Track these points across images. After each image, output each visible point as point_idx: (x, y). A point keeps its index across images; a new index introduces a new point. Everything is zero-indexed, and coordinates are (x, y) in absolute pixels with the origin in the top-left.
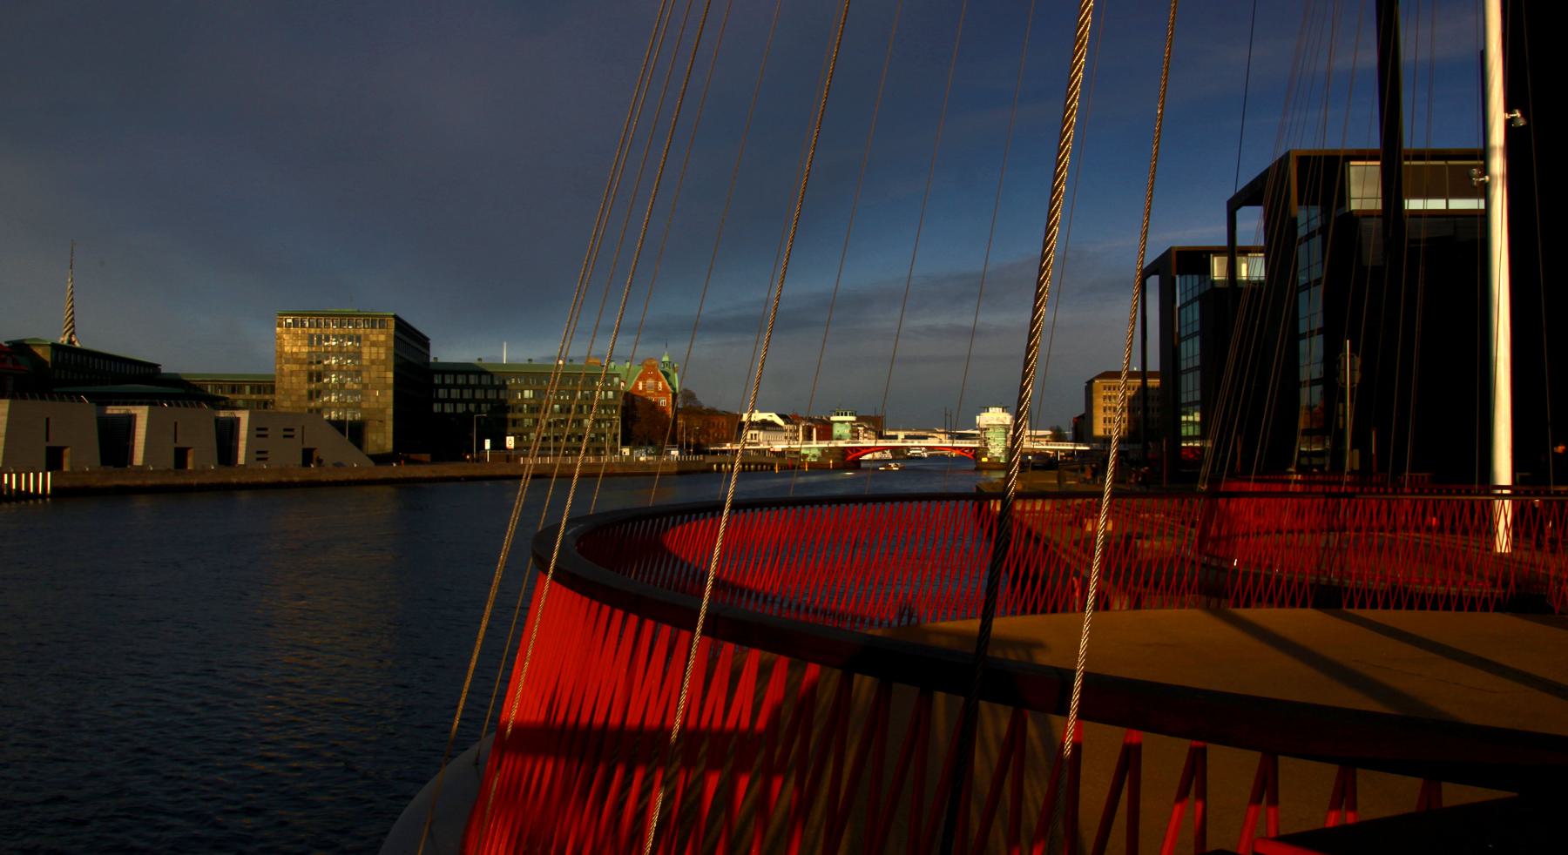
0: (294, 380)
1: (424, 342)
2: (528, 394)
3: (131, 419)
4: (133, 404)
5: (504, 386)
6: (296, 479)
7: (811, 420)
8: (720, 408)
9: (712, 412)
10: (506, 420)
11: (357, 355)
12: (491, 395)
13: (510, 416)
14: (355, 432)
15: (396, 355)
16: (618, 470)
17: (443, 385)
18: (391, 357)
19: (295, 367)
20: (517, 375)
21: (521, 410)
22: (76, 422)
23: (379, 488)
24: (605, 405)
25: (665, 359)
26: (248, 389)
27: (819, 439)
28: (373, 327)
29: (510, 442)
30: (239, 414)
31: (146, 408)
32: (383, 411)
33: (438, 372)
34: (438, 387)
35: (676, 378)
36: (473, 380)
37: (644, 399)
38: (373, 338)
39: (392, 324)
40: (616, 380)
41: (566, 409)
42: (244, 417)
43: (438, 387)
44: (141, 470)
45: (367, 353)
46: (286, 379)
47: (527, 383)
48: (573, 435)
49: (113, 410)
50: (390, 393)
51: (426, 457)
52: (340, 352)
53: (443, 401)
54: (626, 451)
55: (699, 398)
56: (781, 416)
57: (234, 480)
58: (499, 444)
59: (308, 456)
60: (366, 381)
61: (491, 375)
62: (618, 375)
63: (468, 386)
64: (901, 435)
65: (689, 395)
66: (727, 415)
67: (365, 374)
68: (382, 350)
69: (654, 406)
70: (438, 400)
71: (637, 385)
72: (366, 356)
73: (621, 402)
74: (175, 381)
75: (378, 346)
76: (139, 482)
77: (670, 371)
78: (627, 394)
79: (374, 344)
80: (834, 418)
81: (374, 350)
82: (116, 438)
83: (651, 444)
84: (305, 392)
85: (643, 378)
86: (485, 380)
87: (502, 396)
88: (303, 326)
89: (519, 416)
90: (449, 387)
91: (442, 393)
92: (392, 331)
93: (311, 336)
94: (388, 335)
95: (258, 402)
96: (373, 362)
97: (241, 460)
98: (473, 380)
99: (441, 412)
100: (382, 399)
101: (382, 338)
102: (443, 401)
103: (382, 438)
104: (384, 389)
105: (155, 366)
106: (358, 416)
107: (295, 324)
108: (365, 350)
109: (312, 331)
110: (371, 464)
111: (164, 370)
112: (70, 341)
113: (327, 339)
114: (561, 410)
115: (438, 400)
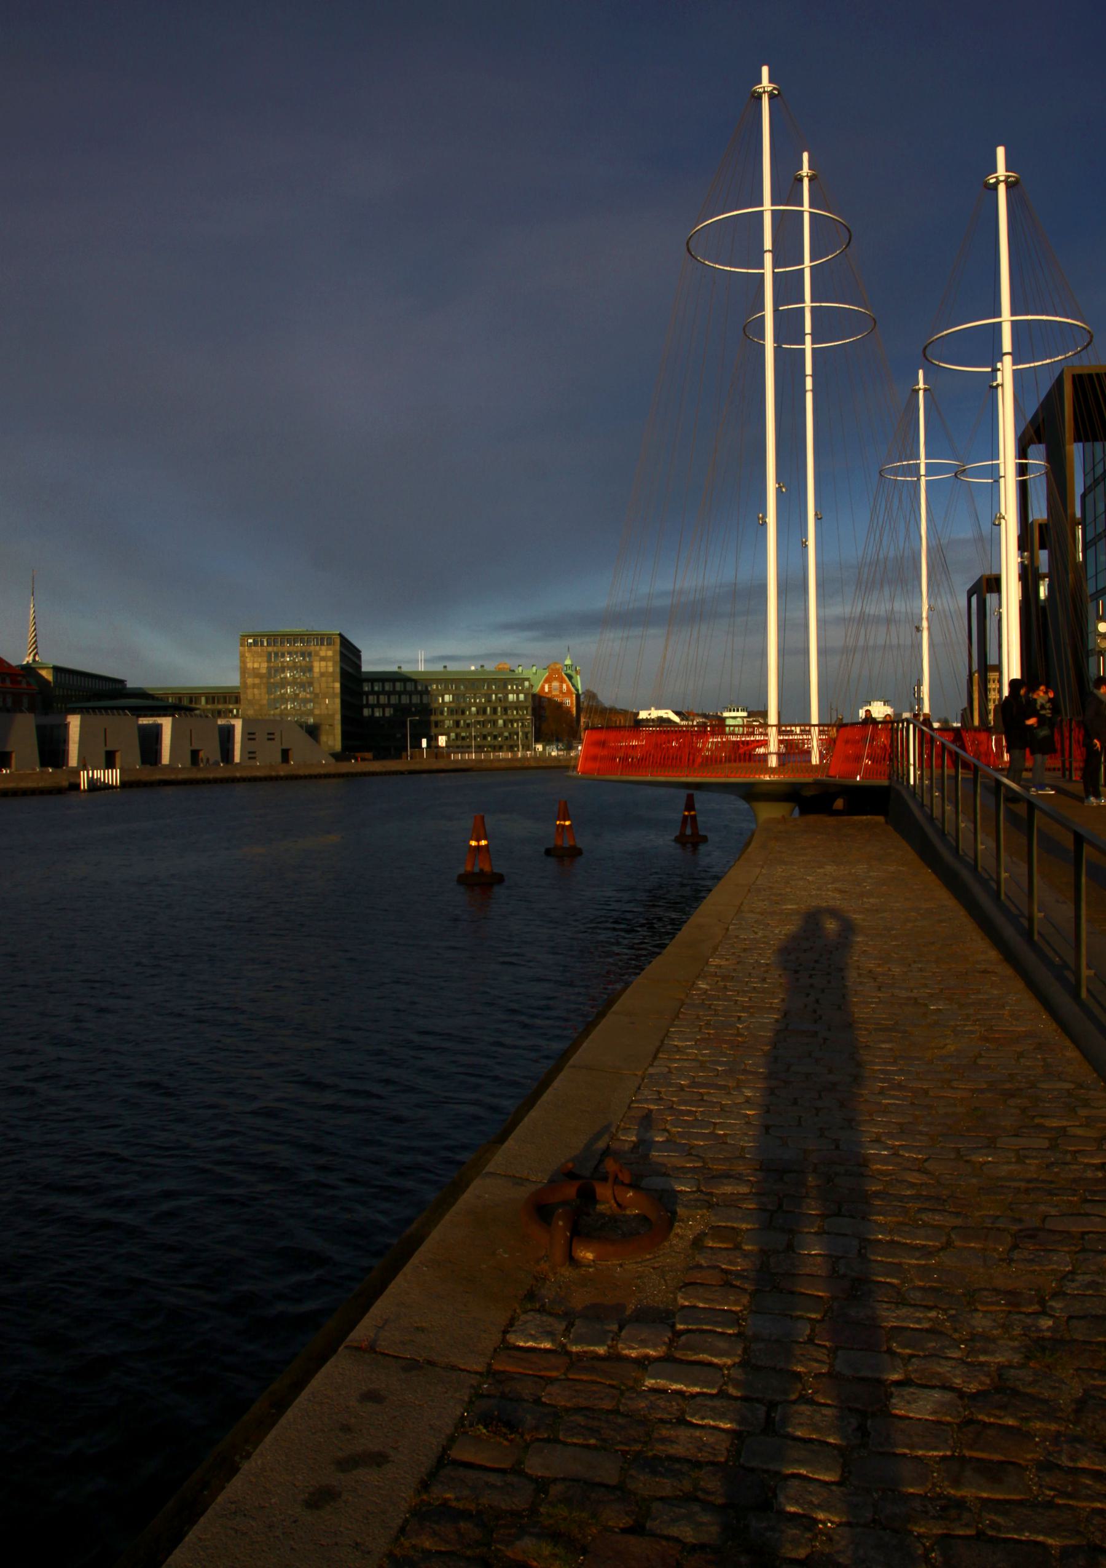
0: (256, 691)
1: (357, 653)
2: (448, 698)
3: (159, 727)
4: (159, 716)
5: (427, 692)
6: (282, 773)
7: (705, 716)
8: (620, 706)
9: (613, 711)
10: (429, 723)
11: (310, 669)
12: (416, 699)
13: (433, 718)
14: (313, 731)
15: (342, 669)
16: (533, 764)
17: (373, 692)
18: (338, 670)
19: (257, 681)
20: (438, 681)
21: (442, 713)
22: (124, 730)
23: (335, 781)
24: (517, 706)
25: (568, 662)
26: (203, 700)
27: (773, 211)
28: (322, 644)
29: (442, 741)
30: (234, 722)
31: (170, 719)
32: (332, 716)
33: (367, 680)
34: (367, 694)
35: (578, 680)
36: (399, 686)
37: (550, 700)
38: (322, 653)
39: (338, 641)
40: (527, 684)
41: (482, 711)
42: (238, 724)
43: (367, 694)
44: (170, 768)
45: (318, 667)
46: (249, 691)
47: (446, 688)
48: (489, 734)
49: (144, 721)
50: (338, 701)
51: (369, 755)
52: (293, 667)
53: (373, 707)
54: (540, 747)
55: (600, 697)
56: (677, 713)
57: (238, 775)
58: (433, 740)
59: (285, 755)
60: (317, 691)
61: (415, 681)
62: (528, 679)
63: (394, 692)
64: (798, 730)
65: (591, 696)
66: (624, 712)
67: (316, 685)
68: (330, 664)
69: (559, 706)
70: (368, 706)
71: (543, 687)
72: (316, 670)
73: (529, 704)
74: (141, 694)
75: (325, 664)
76: (173, 777)
77: (573, 674)
78: (534, 696)
79: (323, 659)
80: (726, 714)
81: (323, 664)
82: (150, 739)
83: (558, 740)
84: (265, 702)
85: (548, 680)
86: (410, 687)
87: (425, 701)
88: (262, 645)
89: (440, 718)
90: (378, 694)
91: (372, 699)
92: (338, 647)
93: (270, 654)
94: (334, 652)
95: (213, 711)
96: (322, 674)
97: (237, 759)
98: (399, 686)
99: (383, 717)
100: (331, 706)
101: (330, 653)
102: (373, 707)
103: (333, 739)
104: (332, 696)
105: (122, 682)
106: (311, 721)
107: (255, 643)
108: (316, 665)
109: (270, 649)
110: (332, 760)
111: (129, 685)
112: (34, 660)
113: (283, 656)
114: (478, 712)
115: (368, 706)
